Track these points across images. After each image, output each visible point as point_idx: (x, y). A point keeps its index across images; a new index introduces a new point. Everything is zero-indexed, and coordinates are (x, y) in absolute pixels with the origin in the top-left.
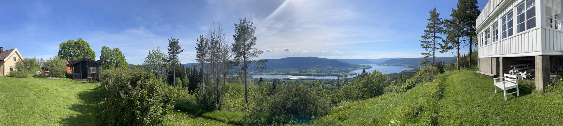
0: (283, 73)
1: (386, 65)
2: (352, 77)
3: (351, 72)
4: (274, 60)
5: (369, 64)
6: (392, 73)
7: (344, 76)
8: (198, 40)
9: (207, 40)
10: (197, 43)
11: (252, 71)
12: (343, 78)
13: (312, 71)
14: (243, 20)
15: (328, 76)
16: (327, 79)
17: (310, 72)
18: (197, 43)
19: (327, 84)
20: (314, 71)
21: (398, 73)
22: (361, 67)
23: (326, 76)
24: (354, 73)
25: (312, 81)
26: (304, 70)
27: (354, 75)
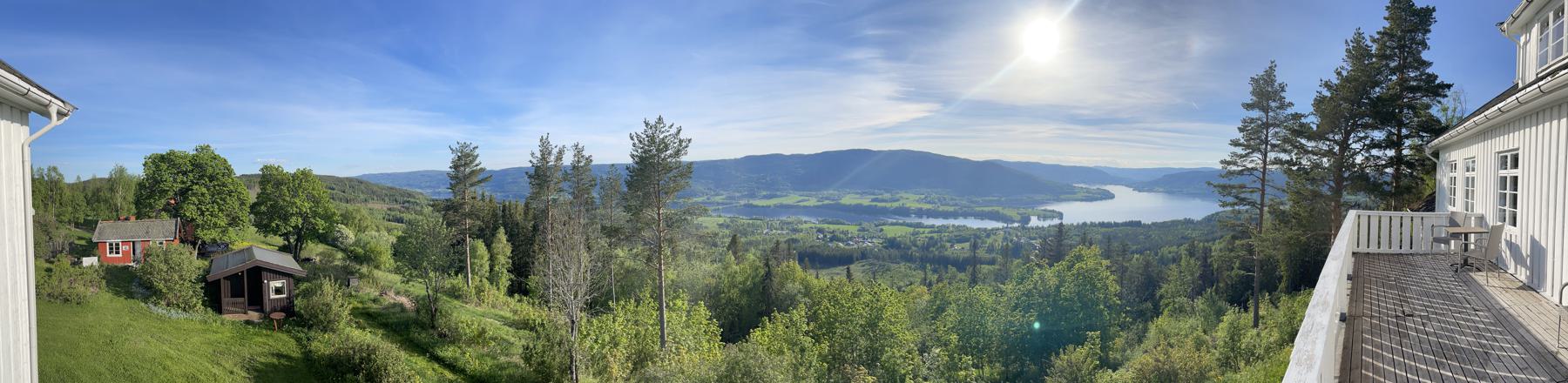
0: (818, 201)
1: (1161, 190)
2: (1046, 224)
3: (1043, 208)
4: (792, 156)
5: (1106, 184)
6: (1180, 219)
7: (1019, 218)
8: (533, 154)
9: (561, 153)
10: (531, 161)
11: (722, 192)
12: (1016, 225)
13: (913, 197)
14: (652, 122)
15: (965, 215)
16: (959, 226)
17: (904, 201)
18: (531, 161)
19: (959, 241)
20: (917, 197)
21: (1199, 219)
22: (1075, 193)
23: (955, 215)
24: (1053, 211)
25: (911, 230)
26: (887, 196)
27: (1053, 217)
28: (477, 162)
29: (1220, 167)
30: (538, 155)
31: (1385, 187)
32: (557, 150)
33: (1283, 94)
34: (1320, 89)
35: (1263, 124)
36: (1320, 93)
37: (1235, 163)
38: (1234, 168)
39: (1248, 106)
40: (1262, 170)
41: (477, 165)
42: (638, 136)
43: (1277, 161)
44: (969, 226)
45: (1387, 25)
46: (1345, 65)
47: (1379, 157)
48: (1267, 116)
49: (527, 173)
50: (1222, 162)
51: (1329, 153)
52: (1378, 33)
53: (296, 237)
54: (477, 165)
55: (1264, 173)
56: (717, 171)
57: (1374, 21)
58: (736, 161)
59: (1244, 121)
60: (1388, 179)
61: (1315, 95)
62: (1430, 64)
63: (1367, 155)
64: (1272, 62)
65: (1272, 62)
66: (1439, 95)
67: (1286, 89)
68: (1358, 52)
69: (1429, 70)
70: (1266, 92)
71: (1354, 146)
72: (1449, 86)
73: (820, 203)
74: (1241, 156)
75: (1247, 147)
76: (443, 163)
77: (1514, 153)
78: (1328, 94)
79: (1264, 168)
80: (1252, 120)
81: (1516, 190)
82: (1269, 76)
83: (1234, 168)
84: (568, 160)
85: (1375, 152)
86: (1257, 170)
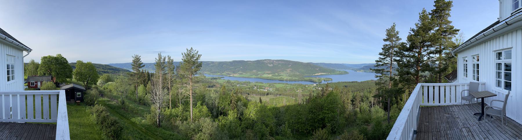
8: (156, 59)
9: (165, 58)
28: (140, 61)
29: (375, 62)
30: (158, 59)
31: (436, 69)
32: (163, 57)
33: (398, 35)
34: (410, 31)
35: (391, 47)
36: (410, 33)
37: (381, 61)
38: (381, 63)
39: (385, 40)
40: (390, 64)
41: (140, 62)
42: (185, 54)
43: (395, 60)
44: (303, 84)
45: (435, 8)
46: (419, 22)
47: (433, 57)
48: (392, 43)
49: (154, 65)
50: (376, 61)
51: (413, 56)
52: (432, 11)
53: (86, 82)
54: (140, 62)
55: (391, 65)
56: (209, 64)
57: (430, 7)
58: (230, 62)
59: (384, 46)
60: (437, 66)
61: (408, 34)
62: (451, 22)
63: (428, 56)
64: (394, 24)
65: (394, 24)
66: (455, 34)
67: (399, 33)
68: (423, 17)
69: (451, 25)
70: (391, 35)
71: (423, 53)
72: (458, 30)
73: (256, 77)
74: (383, 59)
75: (384, 55)
76: (130, 60)
77: (478, 55)
78: (413, 34)
79: (391, 63)
80: (387, 45)
81: (478, 68)
82: (393, 28)
83: (381, 63)
84: (167, 60)
85: (431, 55)
86: (388, 64)
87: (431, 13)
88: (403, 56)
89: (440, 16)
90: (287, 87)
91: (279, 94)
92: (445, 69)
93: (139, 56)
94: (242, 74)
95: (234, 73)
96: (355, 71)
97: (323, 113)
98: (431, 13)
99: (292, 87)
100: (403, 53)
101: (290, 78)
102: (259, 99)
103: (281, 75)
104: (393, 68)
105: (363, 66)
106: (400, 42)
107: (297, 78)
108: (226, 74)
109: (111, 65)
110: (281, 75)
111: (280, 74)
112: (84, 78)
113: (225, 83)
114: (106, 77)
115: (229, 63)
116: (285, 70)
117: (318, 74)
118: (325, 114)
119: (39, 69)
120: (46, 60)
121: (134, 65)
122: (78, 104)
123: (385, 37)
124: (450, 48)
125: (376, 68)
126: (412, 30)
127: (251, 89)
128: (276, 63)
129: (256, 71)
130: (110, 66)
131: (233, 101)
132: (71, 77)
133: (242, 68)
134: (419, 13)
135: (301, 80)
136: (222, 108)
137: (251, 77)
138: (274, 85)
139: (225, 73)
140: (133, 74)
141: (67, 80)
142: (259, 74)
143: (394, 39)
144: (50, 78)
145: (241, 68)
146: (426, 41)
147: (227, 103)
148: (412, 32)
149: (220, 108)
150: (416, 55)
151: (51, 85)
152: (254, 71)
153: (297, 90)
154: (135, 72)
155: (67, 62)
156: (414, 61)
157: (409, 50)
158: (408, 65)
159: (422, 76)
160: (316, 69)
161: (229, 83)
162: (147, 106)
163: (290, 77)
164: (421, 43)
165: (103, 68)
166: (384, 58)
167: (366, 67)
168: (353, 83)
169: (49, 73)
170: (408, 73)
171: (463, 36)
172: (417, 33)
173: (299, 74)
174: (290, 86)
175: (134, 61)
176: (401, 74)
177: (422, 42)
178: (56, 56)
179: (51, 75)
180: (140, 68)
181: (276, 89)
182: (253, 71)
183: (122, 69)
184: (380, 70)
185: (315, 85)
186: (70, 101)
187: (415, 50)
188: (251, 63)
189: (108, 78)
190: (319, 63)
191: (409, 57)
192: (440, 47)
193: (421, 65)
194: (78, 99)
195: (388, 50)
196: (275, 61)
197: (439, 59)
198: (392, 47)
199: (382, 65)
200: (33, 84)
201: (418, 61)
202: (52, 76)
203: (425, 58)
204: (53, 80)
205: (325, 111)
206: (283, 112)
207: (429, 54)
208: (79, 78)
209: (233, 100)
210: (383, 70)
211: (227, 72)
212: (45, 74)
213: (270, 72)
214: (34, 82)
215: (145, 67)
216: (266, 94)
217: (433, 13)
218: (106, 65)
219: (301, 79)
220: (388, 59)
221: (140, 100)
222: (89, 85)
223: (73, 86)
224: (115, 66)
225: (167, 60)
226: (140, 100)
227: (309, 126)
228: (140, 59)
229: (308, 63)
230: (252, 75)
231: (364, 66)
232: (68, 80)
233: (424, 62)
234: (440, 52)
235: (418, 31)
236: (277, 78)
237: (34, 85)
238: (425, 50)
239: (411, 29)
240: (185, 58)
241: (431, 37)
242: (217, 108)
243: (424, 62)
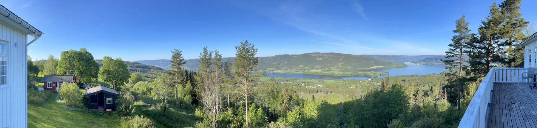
9: (211, 54)
28: (181, 57)
37: (450, 53)
38: (450, 54)
39: (455, 31)
41: (181, 58)
47: (503, 49)
50: (446, 52)
54: (181, 58)
63: (499, 48)
66: (525, 26)
68: (493, 12)
69: (521, 17)
71: (494, 45)
73: (303, 72)
74: (453, 50)
75: (455, 47)
85: (501, 47)
87: (501, 5)
88: (475, 47)
89: (511, 10)
90: (339, 84)
91: (330, 91)
92: (514, 60)
93: (179, 51)
94: (287, 70)
95: (278, 69)
96: (415, 63)
97: (389, 107)
98: (501, 5)
99: (344, 83)
100: (474, 45)
101: (342, 73)
102: (312, 96)
103: (332, 70)
104: (462, 59)
105: (424, 58)
106: (470, 33)
107: (349, 73)
108: (270, 70)
109: (139, 62)
110: (332, 70)
111: (330, 69)
112: (112, 78)
113: (268, 81)
114: (136, 76)
115: (272, 58)
116: (336, 65)
117: (373, 68)
118: (392, 108)
119: (58, 67)
120: (68, 55)
121: (173, 62)
122: (109, 114)
123: (455, 28)
124: (520, 40)
125: (447, 59)
126: (483, 23)
127: (298, 86)
128: (326, 57)
129: (303, 65)
130: (139, 64)
131: (285, 101)
132: (96, 77)
133: (286, 63)
134: (490, 7)
135: (354, 75)
136: (273, 109)
137: (296, 73)
138: (324, 81)
139: (268, 70)
140: (173, 72)
141: (91, 80)
142: (306, 69)
143: (464, 31)
144: (72, 78)
145: (285, 63)
146: (496, 33)
147: (279, 103)
148: (483, 24)
149: (270, 109)
150: (487, 47)
151: (74, 88)
152: (301, 66)
153: (350, 86)
154: (175, 70)
155: (93, 58)
156: (485, 52)
157: (481, 41)
158: (479, 56)
159: (492, 66)
160: (371, 62)
161: (273, 81)
162: (189, 110)
163: (341, 71)
164: (491, 35)
165: (131, 65)
166: (454, 49)
167: (427, 58)
168: (414, 77)
169: (71, 71)
170: (480, 63)
171: (534, 27)
172: (487, 26)
173: (351, 68)
174: (342, 82)
175: (174, 57)
176: (473, 64)
177: (492, 35)
178: (80, 51)
179: (73, 74)
180: (180, 65)
181: (327, 86)
182: (299, 66)
183: (153, 67)
184: (450, 61)
185: (370, 80)
186: (98, 109)
187: (485, 42)
188: (297, 57)
189: (137, 77)
190: (373, 55)
191: (480, 49)
192: (510, 39)
193: (491, 55)
194: (109, 106)
195: (458, 41)
196: (324, 55)
197: (509, 50)
198: (461, 39)
199: (453, 56)
200: (50, 85)
201: (488, 52)
202: (74, 75)
203: (496, 50)
204: (76, 80)
205: (391, 105)
206: (341, 110)
207: (499, 45)
208: (107, 78)
209: (285, 99)
210: (453, 61)
211: (270, 69)
212: (65, 73)
213: (319, 67)
214: (51, 82)
215: (186, 64)
216: (315, 91)
217: (503, 5)
218: (134, 63)
219: (354, 74)
220: (458, 50)
221: (181, 103)
222: (118, 86)
223: (101, 90)
224: (144, 64)
225: (213, 56)
226: (181, 103)
227: (375, 122)
228: (181, 54)
229: (361, 56)
230: (298, 70)
231: (425, 57)
232: (93, 80)
233: (494, 53)
234: (510, 44)
235: (488, 24)
236: (327, 73)
237: (51, 86)
238: (496, 42)
239: (482, 22)
240: (239, 53)
241: (501, 30)
242: (267, 109)
243: (495, 54)
